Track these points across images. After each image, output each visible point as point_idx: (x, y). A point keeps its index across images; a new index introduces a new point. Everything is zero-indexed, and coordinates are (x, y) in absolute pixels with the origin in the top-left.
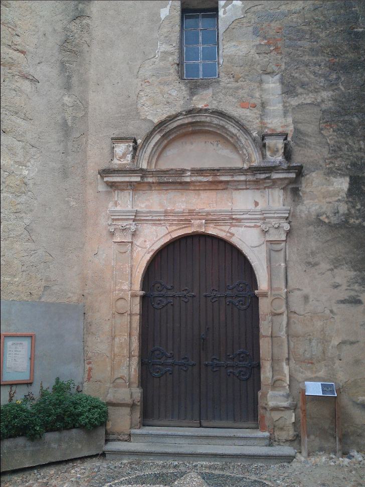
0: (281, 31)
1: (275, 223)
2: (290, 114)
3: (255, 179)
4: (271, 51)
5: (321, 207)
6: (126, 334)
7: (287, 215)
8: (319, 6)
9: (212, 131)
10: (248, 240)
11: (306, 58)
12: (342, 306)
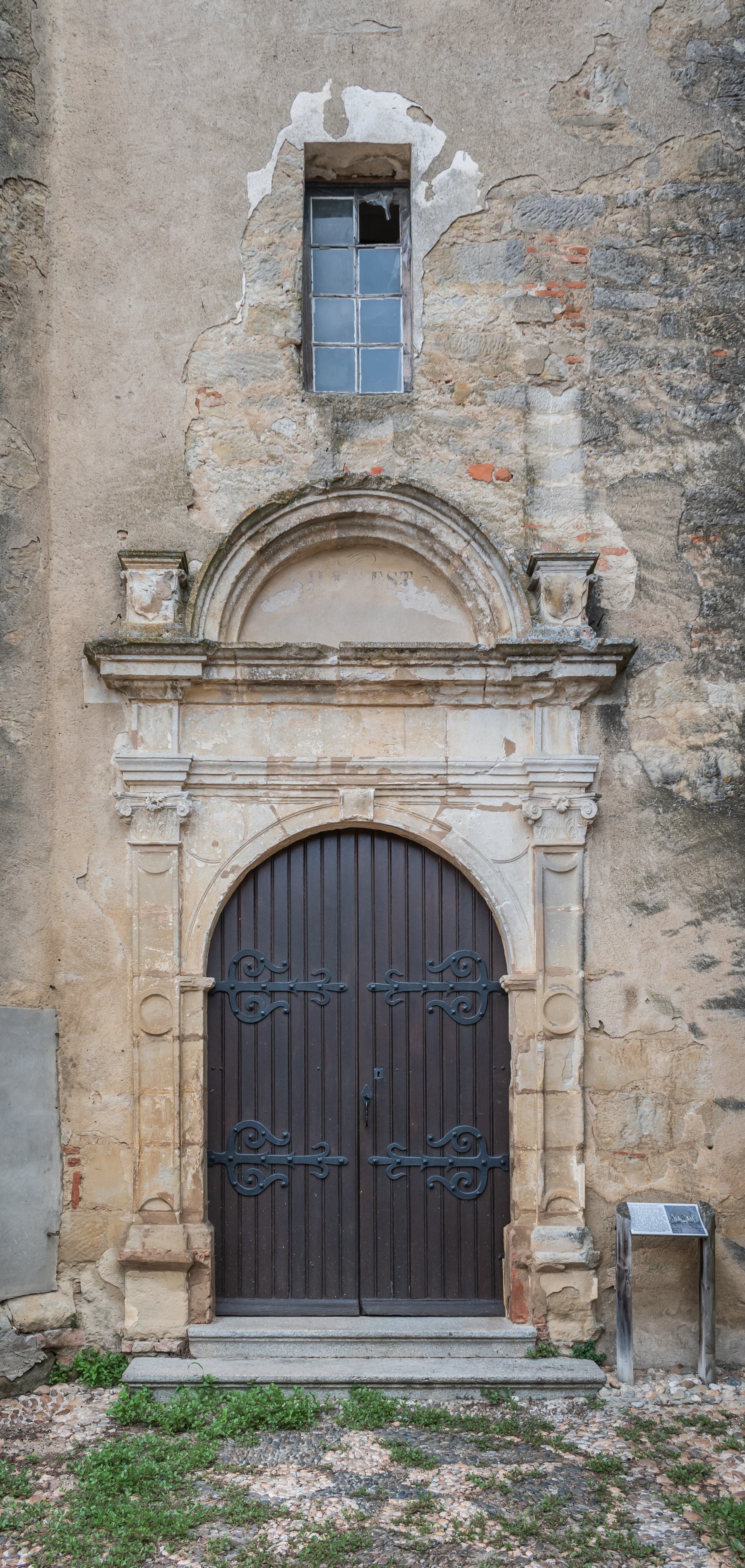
0: (582, 259)
1: (555, 795)
2: (601, 503)
3: (509, 678)
4: (556, 318)
5: (673, 760)
6: (170, 1088)
7: (589, 778)
8: (689, 188)
9: (393, 543)
10: (486, 841)
11: (650, 343)
12: (719, 1013)
